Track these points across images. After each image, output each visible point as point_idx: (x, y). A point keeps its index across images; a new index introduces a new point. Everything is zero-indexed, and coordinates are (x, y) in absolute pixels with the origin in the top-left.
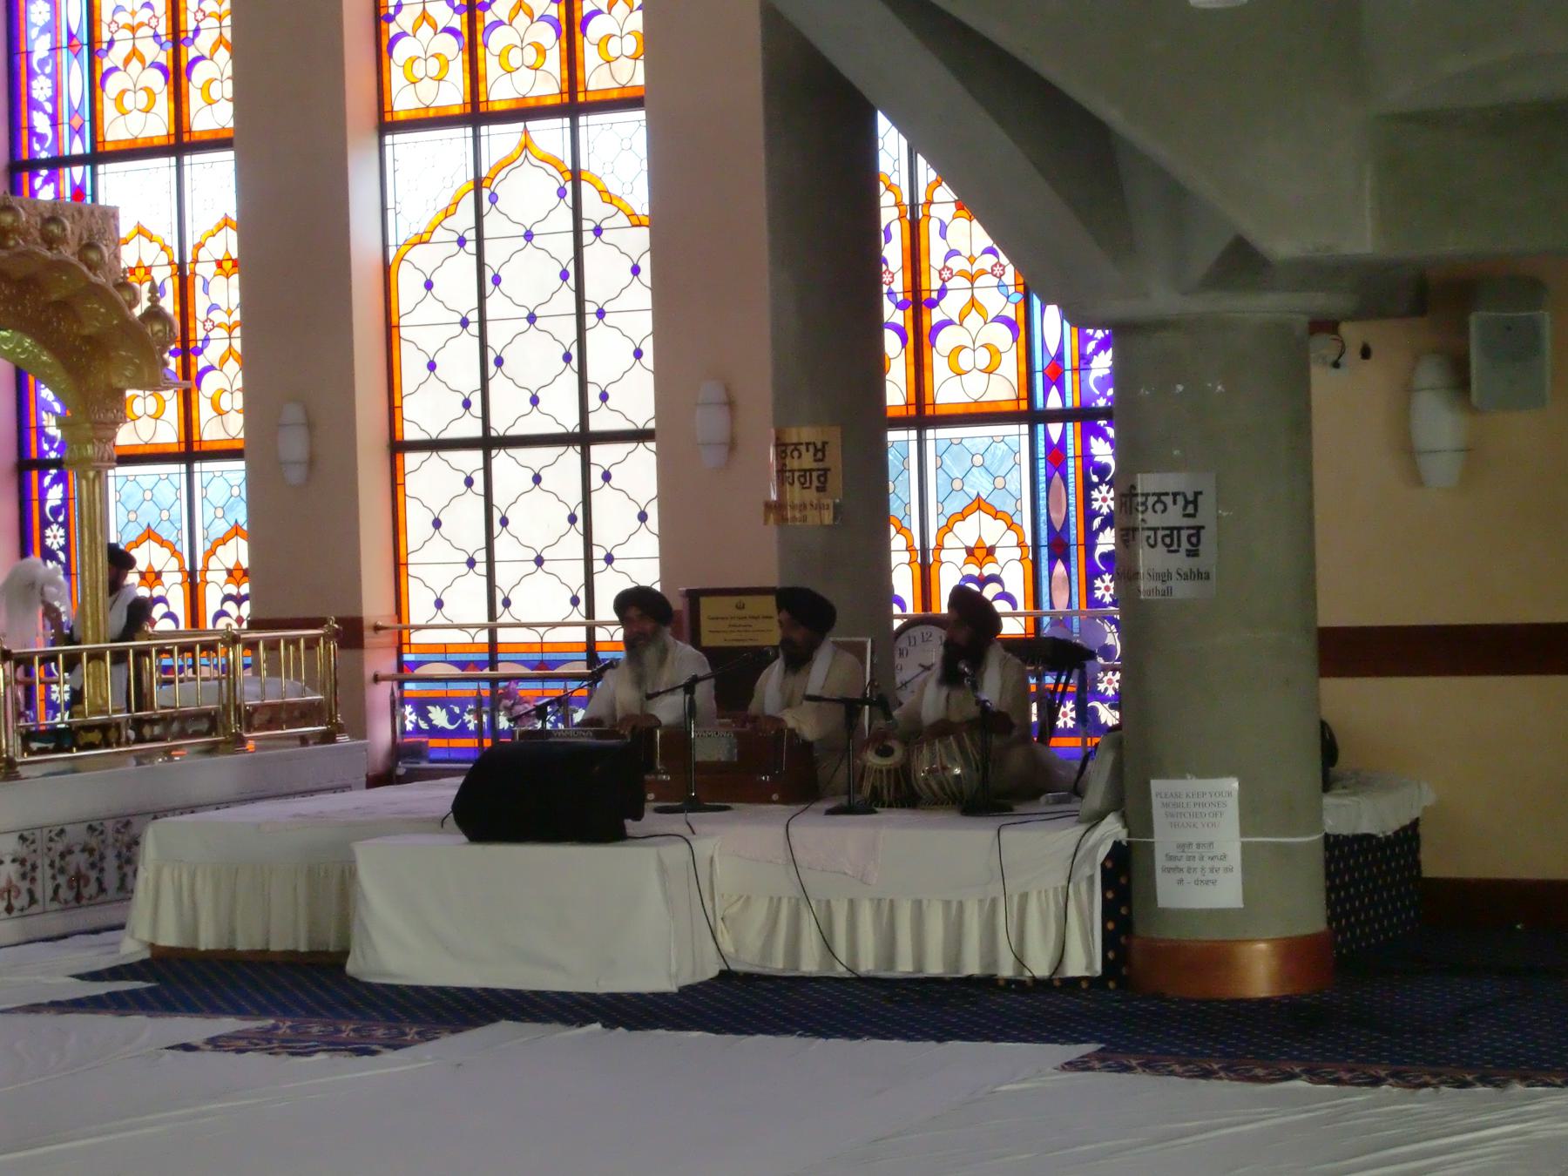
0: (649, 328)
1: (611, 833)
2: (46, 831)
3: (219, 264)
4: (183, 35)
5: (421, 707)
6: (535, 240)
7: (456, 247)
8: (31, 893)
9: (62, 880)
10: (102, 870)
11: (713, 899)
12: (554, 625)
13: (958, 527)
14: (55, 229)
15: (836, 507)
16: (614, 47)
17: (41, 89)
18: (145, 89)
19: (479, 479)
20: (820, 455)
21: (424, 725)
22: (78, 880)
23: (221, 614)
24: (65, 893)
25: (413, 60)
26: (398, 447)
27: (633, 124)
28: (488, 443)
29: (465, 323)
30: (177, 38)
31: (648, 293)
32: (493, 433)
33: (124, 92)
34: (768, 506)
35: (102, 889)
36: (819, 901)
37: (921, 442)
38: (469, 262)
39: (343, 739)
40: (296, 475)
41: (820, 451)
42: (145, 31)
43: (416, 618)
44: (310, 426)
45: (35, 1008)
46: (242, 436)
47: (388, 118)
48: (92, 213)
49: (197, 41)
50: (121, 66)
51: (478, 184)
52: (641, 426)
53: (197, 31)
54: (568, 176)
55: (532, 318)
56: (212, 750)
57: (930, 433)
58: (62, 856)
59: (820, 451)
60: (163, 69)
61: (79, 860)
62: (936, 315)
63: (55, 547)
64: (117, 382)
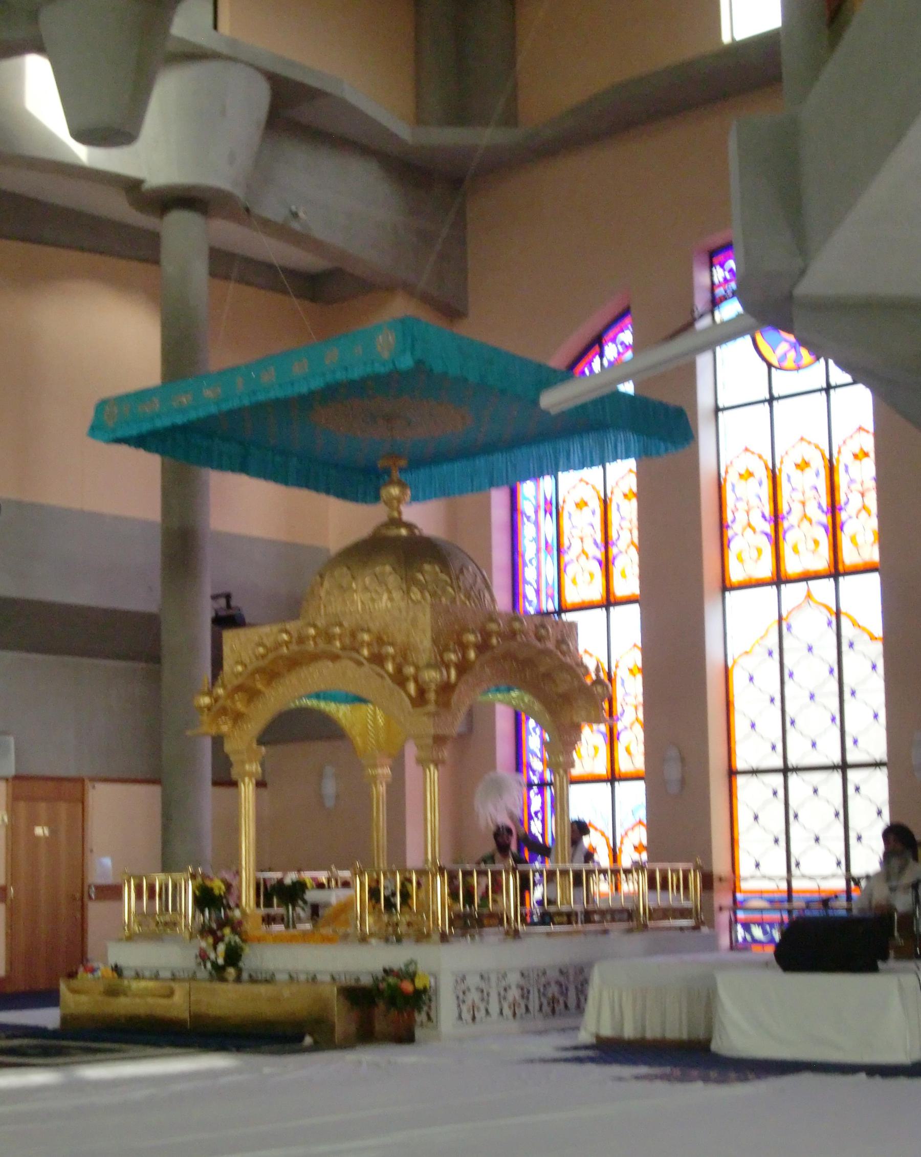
1: (871, 968)
5: (747, 927)
12: (825, 878)
14: (543, 632)
17: (529, 573)
21: (748, 937)
22: (553, 1001)
24: (546, 1008)
26: (717, 410)
35: (566, 1006)
39: (705, 930)
44: (683, 760)
45: (532, 1061)
56: (630, 931)
64: (576, 719)
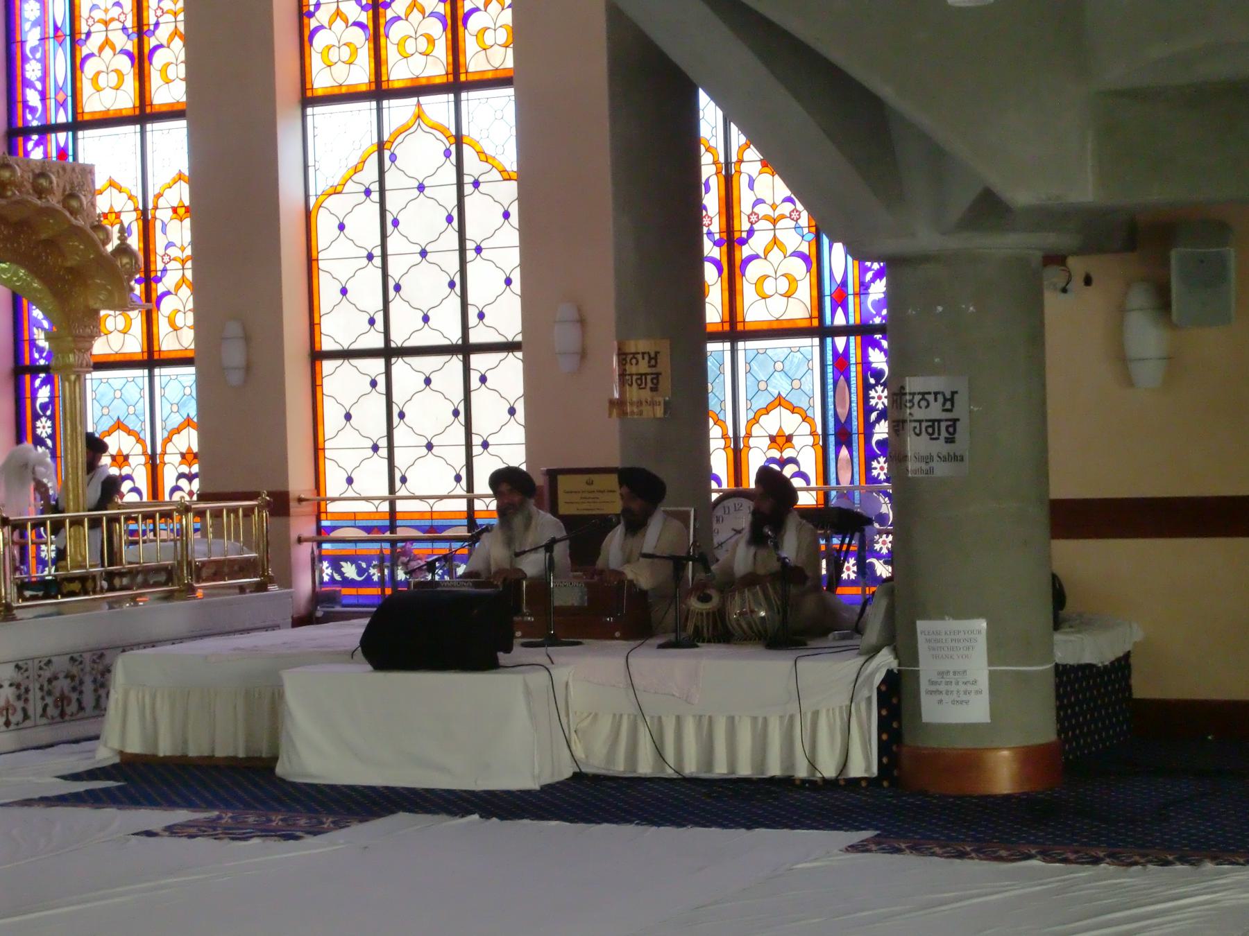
0: (517, 261)
1: (487, 663)
2: (36, 661)
3: (175, 210)
4: (146, 28)
5: (336, 562)
6: (427, 191)
7: (363, 196)
8: (25, 710)
9: (49, 700)
10: (81, 692)
11: (568, 715)
12: (441, 498)
13: (763, 419)
14: (44, 182)
15: (666, 403)
16: (489, 38)
17: (33, 71)
18: (115, 71)
19: (381, 381)
20: (653, 362)
21: (338, 577)
22: (62, 700)
23: (176, 488)
24: (52, 711)
25: (329, 48)
26: (317, 356)
27: (504, 99)
28: (389, 353)
29: (370, 257)
30: (141, 30)
31: (517, 233)
32: (393, 345)
33: (98, 73)
34: (612, 403)
35: (81, 708)
36: (652, 717)
37: (734, 352)
38: (373, 208)
39: (273, 588)
40: (235, 378)
41: (653, 359)
42: (116, 25)
43: (331, 492)
44: (247, 339)
45: (28, 803)
46: (192, 347)
47: (309, 94)
48: (73, 170)
49: (157, 32)
50: (96, 53)
51: (381, 146)
52: (510, 339)
53: (157, 25)
54: (452, 140)
55: (424, 253)
56: (169, 597)
57: (741, 345)
58: (50, 681)
59: (653, 359)
60: (129, 55)
61: (63, 684)
62: (746, 251)
63: (44, 435)
64: (93, 304)
